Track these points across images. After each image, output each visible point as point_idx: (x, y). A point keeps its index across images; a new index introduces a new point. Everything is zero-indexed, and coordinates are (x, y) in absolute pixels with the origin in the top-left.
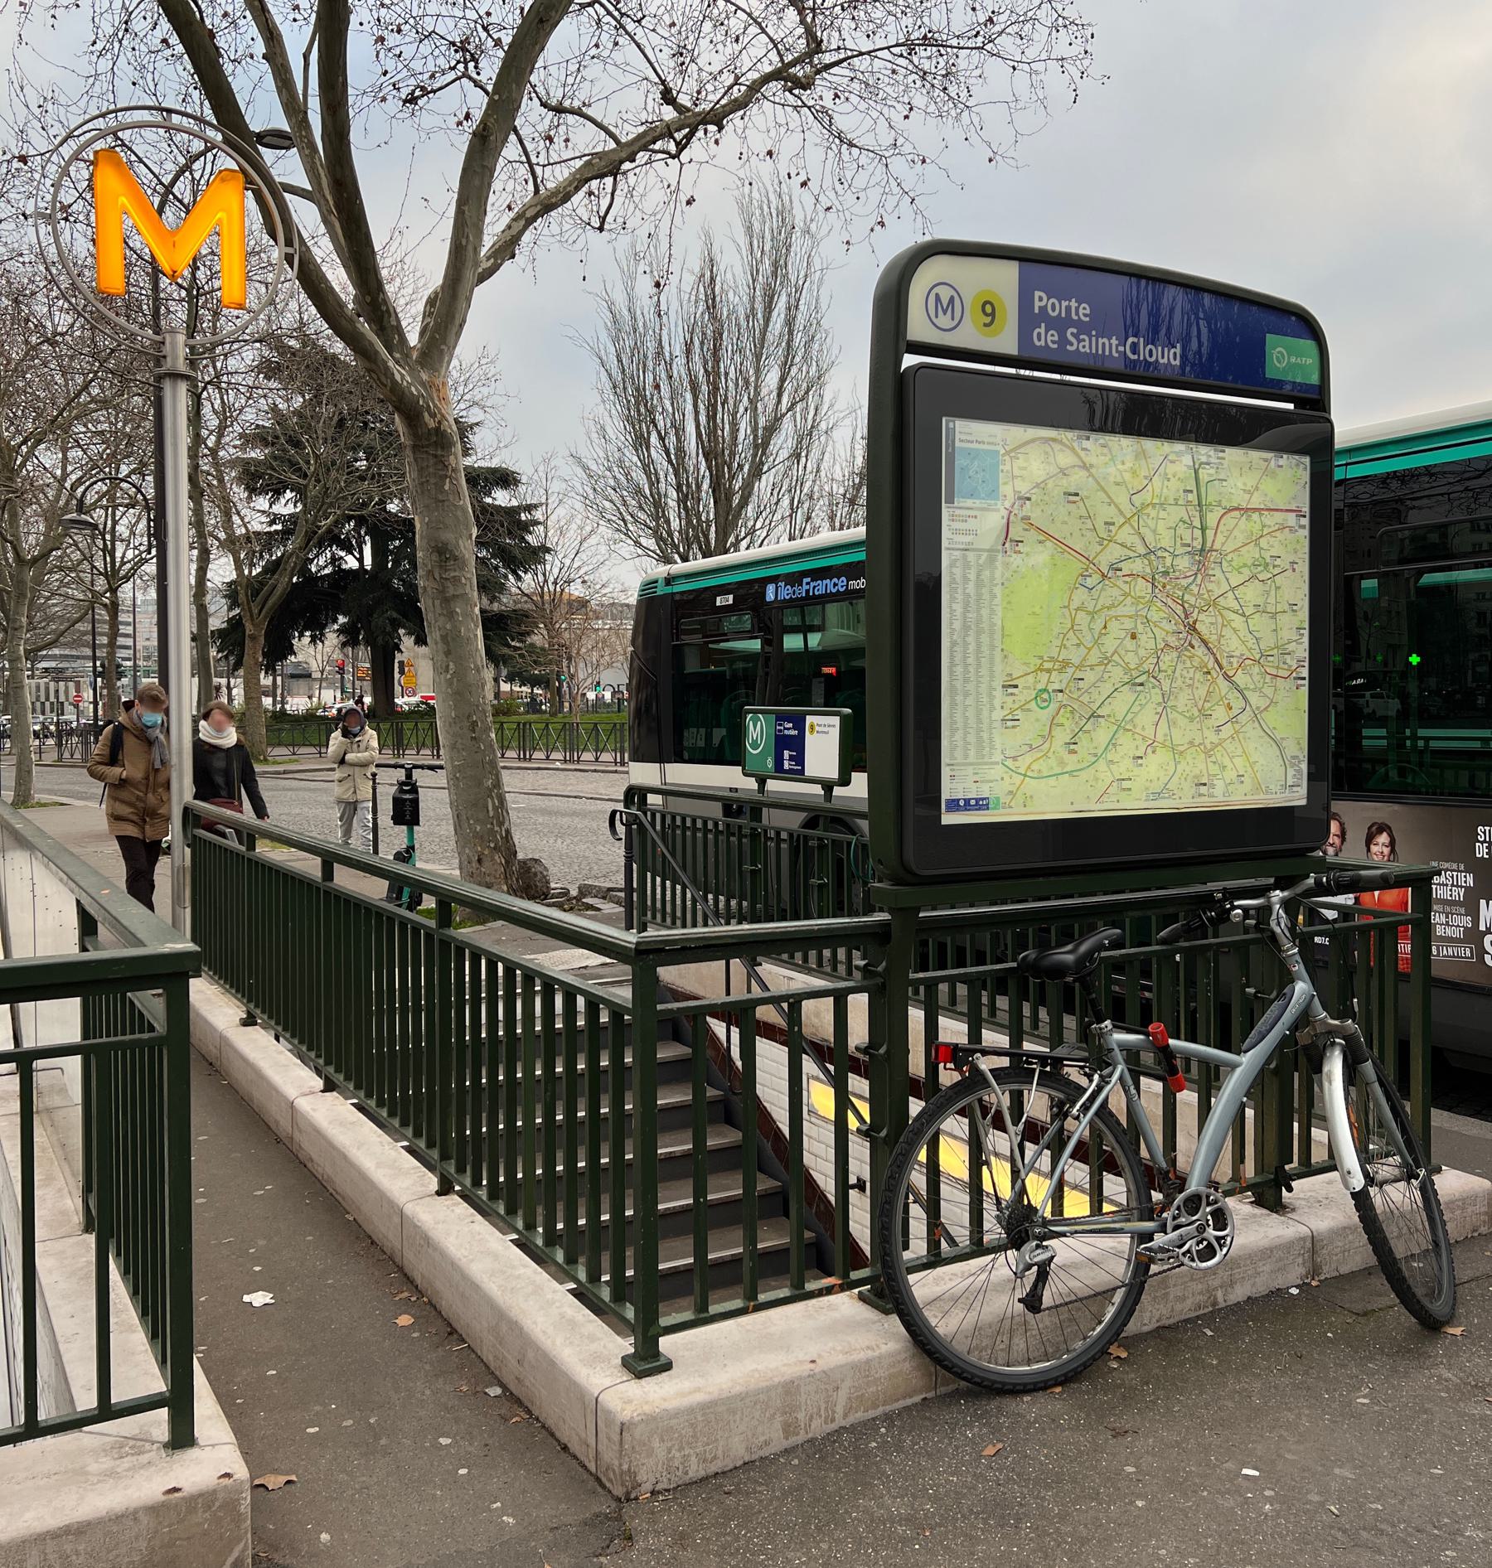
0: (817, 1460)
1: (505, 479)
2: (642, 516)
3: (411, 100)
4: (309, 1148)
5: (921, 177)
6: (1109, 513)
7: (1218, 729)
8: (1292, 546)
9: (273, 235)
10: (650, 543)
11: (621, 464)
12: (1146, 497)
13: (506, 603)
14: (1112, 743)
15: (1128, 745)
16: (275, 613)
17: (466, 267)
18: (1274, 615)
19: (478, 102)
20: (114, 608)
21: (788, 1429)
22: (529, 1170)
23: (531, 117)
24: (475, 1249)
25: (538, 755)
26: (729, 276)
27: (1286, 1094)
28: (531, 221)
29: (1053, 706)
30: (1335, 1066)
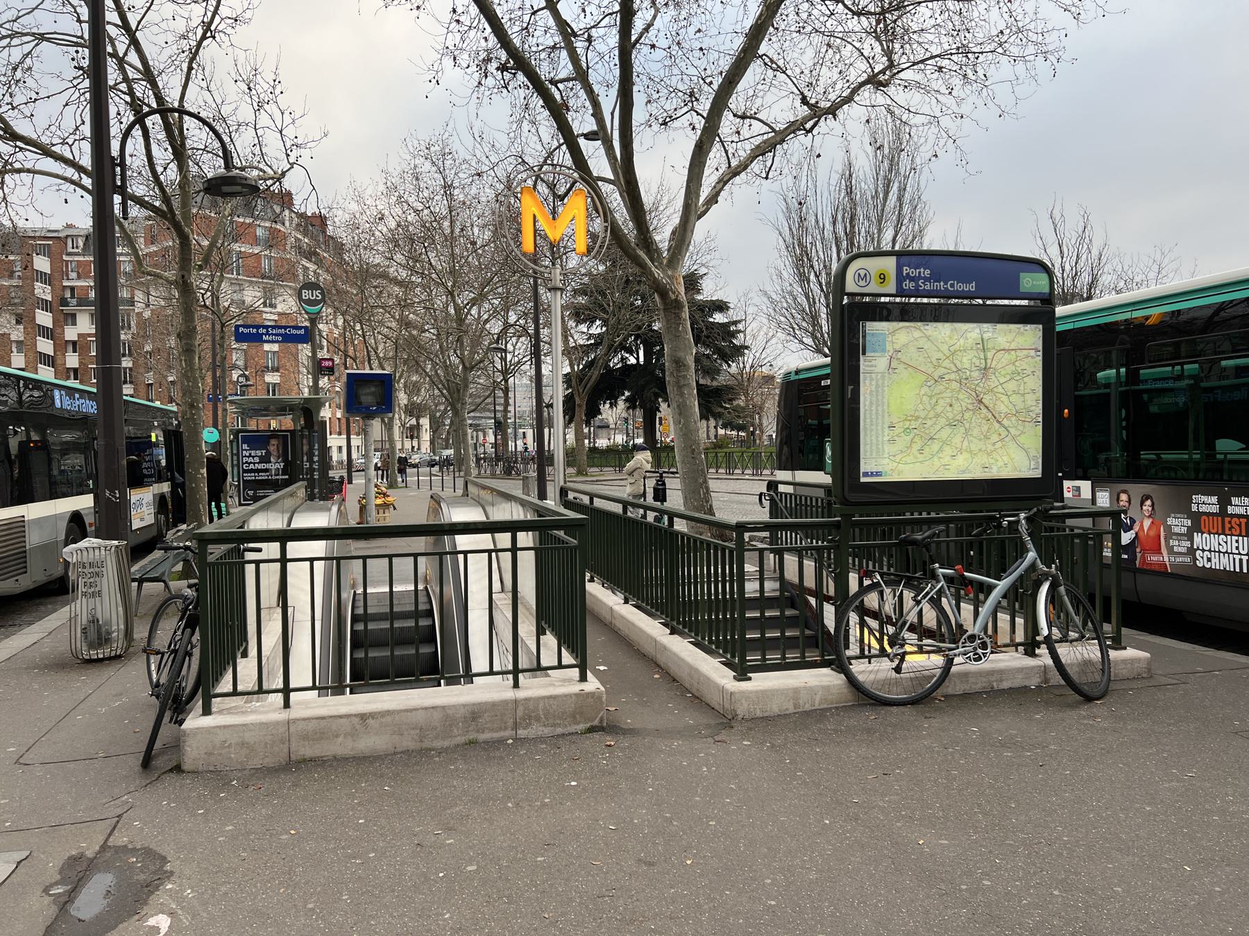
0: (805, 718)
1: (721, 306)
2: (804, 324)
3: (665, 123)
4: (619, 624)
5: (959, 128)
6: (940, 355)
7: (994, 444)
8: (1035, 364)
9: (597, 212)
10: (809, 341)
11: (791, 293)
12: (956, 347)
13: (722, 380)
14: (941, 450)
15: (948, 451)
16: (592, 390)
17: (691, 212)
18: (1023, 395)
19: (700, 123)
20: (506, 391)
21: (796, 706)
22: (703, 617)
23: (727, 124)
24: (682, 649)
25: (736, 471)
26: (861, 173)
27: (1021, 599)
28: (726, 183)
29: (912, 435)
30: (1045, 588)
